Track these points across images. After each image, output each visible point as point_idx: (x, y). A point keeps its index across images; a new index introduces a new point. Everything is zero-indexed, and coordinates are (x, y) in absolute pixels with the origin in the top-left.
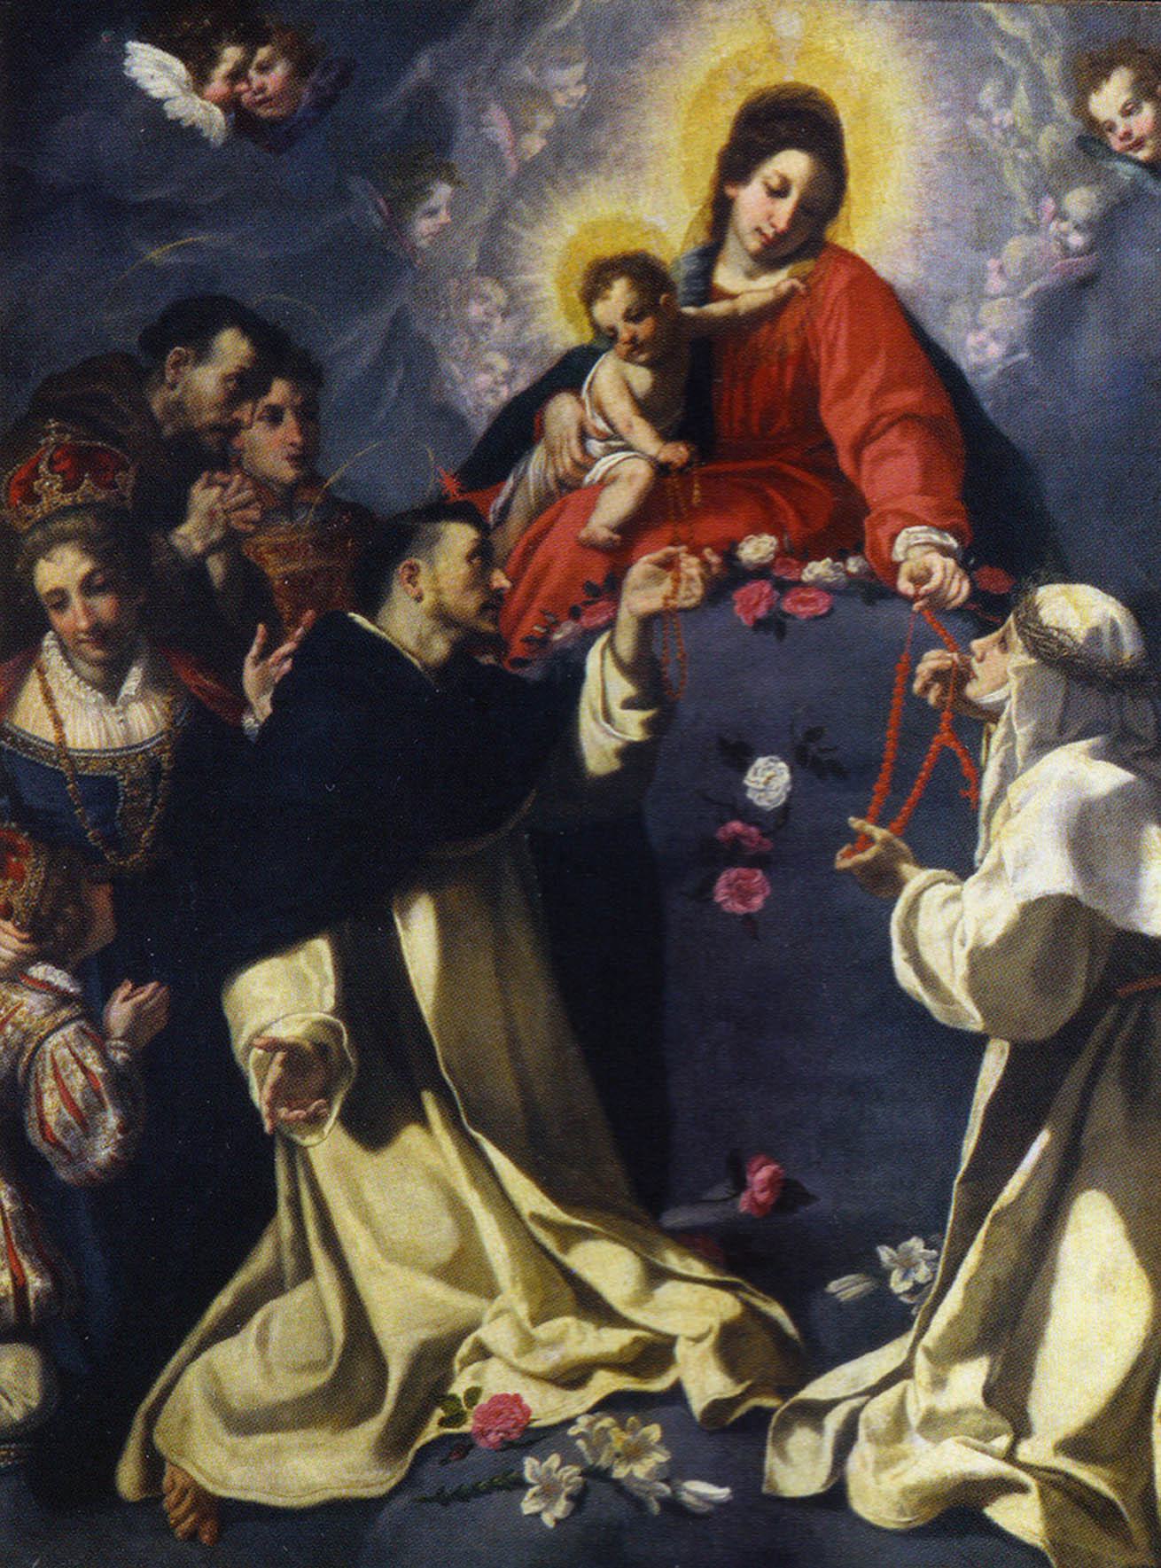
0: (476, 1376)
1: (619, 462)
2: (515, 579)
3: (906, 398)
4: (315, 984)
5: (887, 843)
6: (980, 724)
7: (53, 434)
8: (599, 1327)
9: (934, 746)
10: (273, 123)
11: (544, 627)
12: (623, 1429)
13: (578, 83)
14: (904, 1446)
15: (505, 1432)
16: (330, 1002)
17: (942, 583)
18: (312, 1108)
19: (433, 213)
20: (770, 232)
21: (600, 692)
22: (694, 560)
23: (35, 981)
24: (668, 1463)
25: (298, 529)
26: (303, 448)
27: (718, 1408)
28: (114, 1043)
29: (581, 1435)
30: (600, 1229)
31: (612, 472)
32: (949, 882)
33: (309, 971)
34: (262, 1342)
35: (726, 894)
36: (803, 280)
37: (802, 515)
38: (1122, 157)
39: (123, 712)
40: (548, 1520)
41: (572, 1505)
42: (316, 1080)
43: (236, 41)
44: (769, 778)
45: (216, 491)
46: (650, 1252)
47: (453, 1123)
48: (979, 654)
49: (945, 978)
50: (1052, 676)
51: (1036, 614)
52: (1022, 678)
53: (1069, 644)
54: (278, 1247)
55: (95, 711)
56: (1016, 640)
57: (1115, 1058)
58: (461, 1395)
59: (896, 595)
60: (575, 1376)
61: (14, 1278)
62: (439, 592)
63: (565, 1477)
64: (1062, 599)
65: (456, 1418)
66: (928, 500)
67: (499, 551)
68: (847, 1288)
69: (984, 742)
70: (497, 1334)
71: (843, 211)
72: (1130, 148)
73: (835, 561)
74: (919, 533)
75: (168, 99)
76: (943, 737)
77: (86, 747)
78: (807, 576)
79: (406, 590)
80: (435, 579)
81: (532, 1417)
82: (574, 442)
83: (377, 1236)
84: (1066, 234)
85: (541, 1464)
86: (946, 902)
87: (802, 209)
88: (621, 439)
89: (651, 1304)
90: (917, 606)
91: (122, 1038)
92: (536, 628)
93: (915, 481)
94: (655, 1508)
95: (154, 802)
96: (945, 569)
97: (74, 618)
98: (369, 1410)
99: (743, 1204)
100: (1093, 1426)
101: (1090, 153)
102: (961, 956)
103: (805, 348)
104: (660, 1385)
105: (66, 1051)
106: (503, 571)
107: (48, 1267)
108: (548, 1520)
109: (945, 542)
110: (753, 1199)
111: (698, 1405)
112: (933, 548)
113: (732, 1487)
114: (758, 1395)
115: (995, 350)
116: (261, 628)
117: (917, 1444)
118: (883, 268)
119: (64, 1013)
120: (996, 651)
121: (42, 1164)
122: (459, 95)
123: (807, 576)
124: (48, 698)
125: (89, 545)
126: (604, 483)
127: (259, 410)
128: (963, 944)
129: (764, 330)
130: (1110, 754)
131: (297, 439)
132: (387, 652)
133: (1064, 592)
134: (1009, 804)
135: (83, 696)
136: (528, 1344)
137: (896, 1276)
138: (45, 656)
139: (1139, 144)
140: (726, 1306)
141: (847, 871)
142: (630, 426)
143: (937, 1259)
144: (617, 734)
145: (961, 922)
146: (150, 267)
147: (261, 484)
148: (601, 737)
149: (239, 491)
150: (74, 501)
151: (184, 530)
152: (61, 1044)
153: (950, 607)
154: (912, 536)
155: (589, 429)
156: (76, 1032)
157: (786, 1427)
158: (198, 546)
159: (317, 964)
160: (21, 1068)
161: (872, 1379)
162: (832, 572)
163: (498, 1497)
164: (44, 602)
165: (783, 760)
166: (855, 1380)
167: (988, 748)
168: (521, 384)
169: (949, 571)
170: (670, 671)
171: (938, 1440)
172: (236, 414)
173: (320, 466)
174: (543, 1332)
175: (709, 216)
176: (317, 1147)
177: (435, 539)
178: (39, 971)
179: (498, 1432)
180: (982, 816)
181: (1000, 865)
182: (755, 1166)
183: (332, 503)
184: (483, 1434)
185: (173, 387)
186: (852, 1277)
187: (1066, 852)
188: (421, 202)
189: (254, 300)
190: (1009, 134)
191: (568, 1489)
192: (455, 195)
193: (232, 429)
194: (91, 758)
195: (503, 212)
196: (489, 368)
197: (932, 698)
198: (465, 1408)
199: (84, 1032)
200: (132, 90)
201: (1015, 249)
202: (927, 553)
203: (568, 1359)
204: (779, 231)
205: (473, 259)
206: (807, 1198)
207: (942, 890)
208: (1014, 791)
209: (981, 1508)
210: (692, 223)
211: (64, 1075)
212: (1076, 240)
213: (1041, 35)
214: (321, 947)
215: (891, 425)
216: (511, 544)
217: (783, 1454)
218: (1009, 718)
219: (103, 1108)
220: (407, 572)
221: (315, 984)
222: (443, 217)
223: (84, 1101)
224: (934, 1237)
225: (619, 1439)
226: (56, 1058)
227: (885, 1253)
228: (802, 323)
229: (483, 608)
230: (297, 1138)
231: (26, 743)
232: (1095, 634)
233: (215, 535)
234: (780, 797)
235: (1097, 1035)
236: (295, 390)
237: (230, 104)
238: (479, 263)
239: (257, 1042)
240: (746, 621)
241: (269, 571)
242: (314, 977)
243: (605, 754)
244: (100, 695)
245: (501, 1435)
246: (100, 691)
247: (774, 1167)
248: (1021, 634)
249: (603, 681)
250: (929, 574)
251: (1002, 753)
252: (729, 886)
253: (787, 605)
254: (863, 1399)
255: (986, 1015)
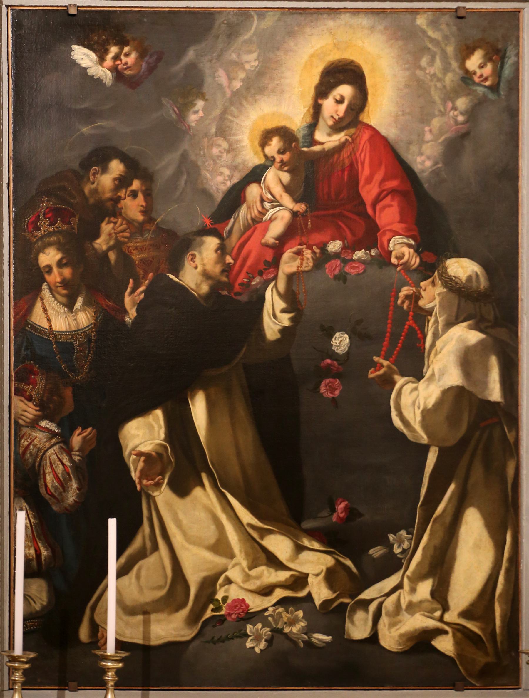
0: (226, 591)
1: (277, 212)
2: (235, 260)
3: (393, 184)
4: (156, 428)
5: (389, 367)
6: (426, 316)
7: (45, 203)
8: (276, 570)
9: (406, 326)
10: (131, 77)
11: (248, 279)
12: (288, 612)
13: (255, 60)
14: (399, 618)
15: (239, 614)
16: (163, 436)
17: (409, 259)
18: (156, 480)
19: (196, 112)
20: (337, 117)
21: (271, 307)
22: (309, 251)
23: (42, 427)
24: (306, 626)
25: (145, 240)
26: (146, 207)
27: (326, 603)
28: (74, 453)
29: (270, 615)
30: (276, 530)
31: (274, 216)
32: (413, 382)
33: (153, 423)
34: (138, 577)
35: (324, 390)
36: (351, 137)
37: (353, 234)
38: (479, 85)
39: (75, 316)
40: (257, 650)
41: (267, 644)
42: (158, 468)
43: (115, 44)
44: (341, 341)
45: (112, 225)
46: (298, 540)
47: (214, 486)
48: (423, 288)
49: (412, 422)
50: (452, 295)
51: (446, 270)
52: (441, 297)
53: (459, 282)
54: (144, 537)
55: (64, 316)
56: (438, 282)
57: (479, 452)
58: (220, 599)
59: (390, 263)
60: (268, 590)
61: (36, 551)
62: (204, 265)
63: (264, 633)
64: (456, 265)
65: (218, 609)
66: (403, 225)
67: (228, 248)
68: (376, 552)
69: (426, 324)
70: (234, 574)
71: (366, 108)
72: (482, 81)
73: (366, 250)
74: (399, 239)
75: (89, 68)
76: (410, 322)
77: (61, 330)
78: (355, 257)
79: (190, 264)
80: (202, 259)
81: (250, 608)
82: (258, 204)
83: (185, 534)
84: (457, 116)
85: (254, 627)
86: (412, 391)
87: (350, 108)
88: (278, 202)
89: (297, 561)
90: (398, 269)
91: (78, 451)
92: (245, 280)
93: (397, 217)
94: (302, 645)
95: (88, 353)
96: (409, 253)
97: (55, 277)
98: (183, 605)
99: (334, 518)
100: (473, 605)
101: (467, 84)
102: (418, 412)
103: (352, 165)
104: (302, 594)
105: (55, 457)
106: (230, 256)
107: (49, 546)
108: (257, 650)
109: (410, 242)
110: (338, 515)
111: (318, 603)
112: (404, 245)
113: (332, 636)
114: (342, 597)
115: (428, 164)
116: (131, 281)
117: (405, 616)
118: (383, 132)
119: (54, 441)
120: (430, 287)
121: (47, 504)
122: (205, 66)
123: (355, 257)
124: (45, 310)
125: (60, 247)
126: (271, 220)
127: (128, 192)
128: (419, 408)
129: (336, 156)
130: (477, 327)
131: (144, 204)
132: (183, 289)
133: (457, 262)
134: (436, 349)
135: (59, 309)
136: (247, 578)
137: (395, 546)
138: (43, 293)
139: (486, 79)
140: (328, 561)
141: (373, 379)
142: (281, 196)
143: (412, 539)
144: (279, 323)
145: (418, 400)
146: (82, 134)
147: (130, 222)
148: (272, 325)
149: (121, 225)
150: (54, 230)
151: (98, 241)
152: (52, 454)
153: (412, 268)
154: (396, 240)
155: (265, 198)
156: (59, 448)
157: (353, 611)
158: (104, 247)
159: (157, 419)
160: (37, 464)
161: (387, 590)
162: (364, 255)
163: (237, 641)
164: (43, 270)
165: (346, 334)
166: (380, 591)
167: (428, 326)
168: (235, 180)
169: (411, 255)
170: (301, 297)
171: (413, 614)
172: (119, 194)
173: (154, 215)
174: (254, 572)
175: (312, 111)
176: (159, 496)
177: (202, 243)
178: (43, 423)
179: (235, 614)
180: (426, 354)
181: (433, 375)
182: (339, 502)
183: (159, 229)
184: (230, 615)
185: (93, 183)
186: (378, 547)
187: (460, 368)
188: (192, 108)
189: (125, 148)
190: (433, 77)
191: (265, 637)
192: (205, 105)
193: (117, 200)
194: (63, 334)
195: (225, 111)
196: (222, 174)
197: (405, 307)
198: (222, 604)
199: (62, 448)
200: (74, 63)
201: (436, 123)
202: (402, 247)
203: (265, 584)
204: (340, 117)
205: (213, 130)
206: (360, 515)
207: (410, 386)
208: (439, 344)
209: (430, 641)
210: (304, 115)
211: (54, 466)
212: (461, 118)
213: (446, 38)
214: (159, 413)
215: (386, 196)
216: (233, 244)
217: (352, 622)
218: (436, 313)
219: (70, 480)
220: (191, 257)
221: (156, 428)
222: (201, 114)
223: (63, 477)
224: (410, 530)
225: (286, 616)
226: (51, 459)
227: (391, 537)
228: (351, 154)
229: (223, 271)
230: (151, 493)
231: (35, 328)
232: (469, 278)
233: (112, 243)
234: (346, 348)
235: (473, 443)
236: (142, 184)
237: (114, 69)
238: (216, 132)
239: (133, 452)
240: (331, 276)
241: (134, 257)
242: (156, 426)
243: (274, 332)
244: (66, 309)
245: (237, 615)
246: (66, 307)
247: (346, 503)
248: (440, 279)
249: (273, 303)
250: (403, 255)
251: (433, 328)
252: (326, 386)
253: (347, 269)
254: (383, 598)
255: (429, 437)
